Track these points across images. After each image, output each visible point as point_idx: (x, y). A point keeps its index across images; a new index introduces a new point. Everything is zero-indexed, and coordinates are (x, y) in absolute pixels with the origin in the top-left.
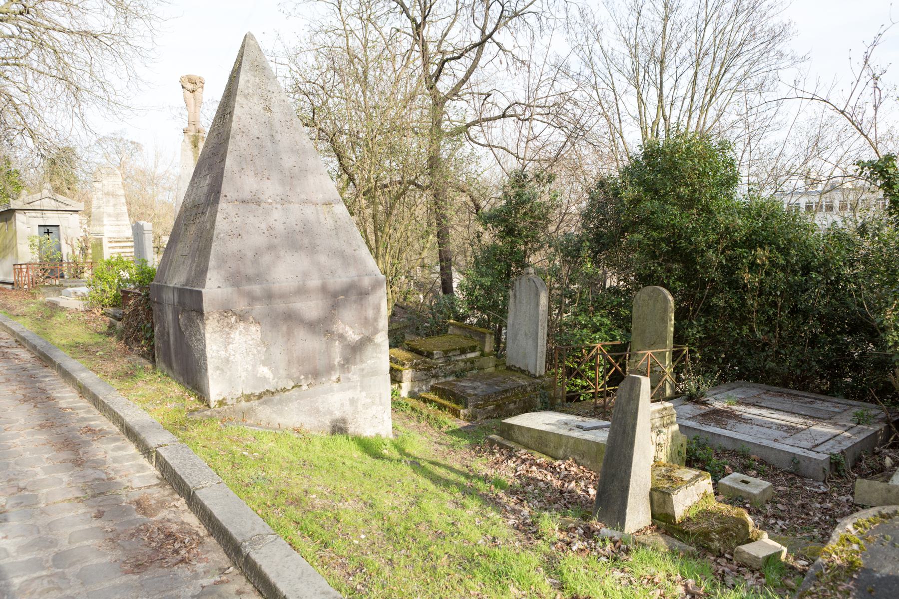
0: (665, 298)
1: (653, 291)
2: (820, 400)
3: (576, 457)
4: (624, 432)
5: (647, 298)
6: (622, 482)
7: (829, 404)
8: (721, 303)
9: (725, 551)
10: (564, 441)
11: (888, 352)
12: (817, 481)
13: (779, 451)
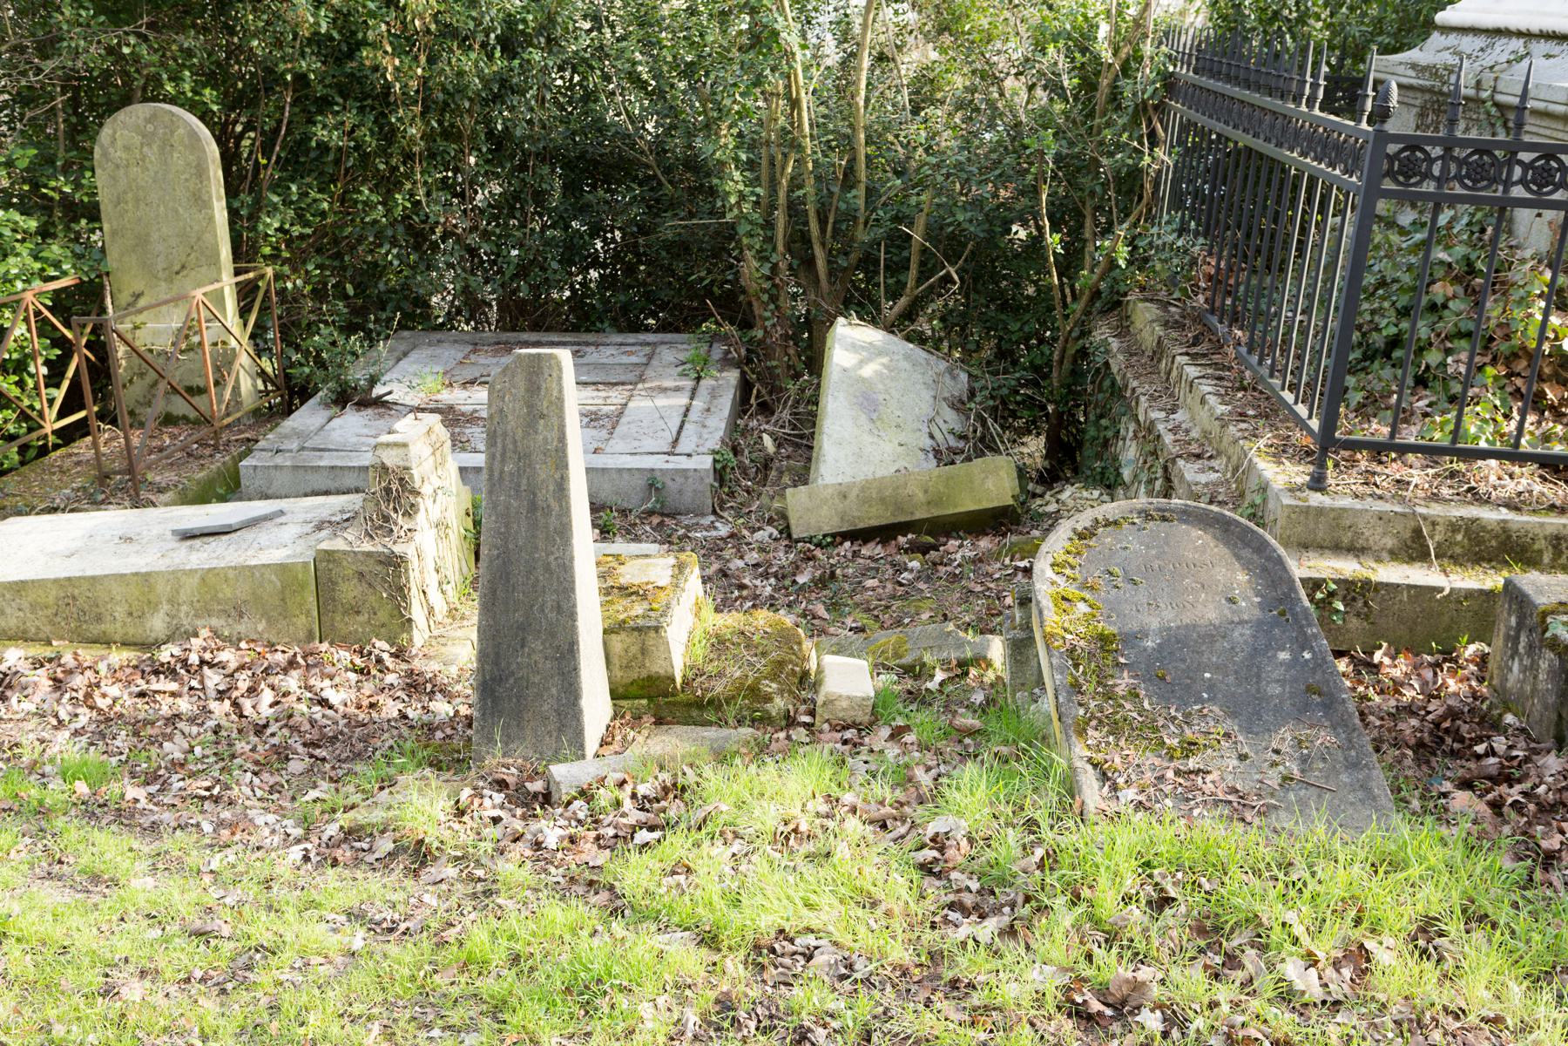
0: (193, 135)
1: (151, 119)
2: (587, 344)
3: (215, 622)
4: (533, 507)
5: (137, 140)
6: (553, 635)
7: (610, 351)
8: (336, 139)
9: (796, 712)
10: (163, 589)
11: (729, 218)
12: (703, 515)
13: (620, 471)
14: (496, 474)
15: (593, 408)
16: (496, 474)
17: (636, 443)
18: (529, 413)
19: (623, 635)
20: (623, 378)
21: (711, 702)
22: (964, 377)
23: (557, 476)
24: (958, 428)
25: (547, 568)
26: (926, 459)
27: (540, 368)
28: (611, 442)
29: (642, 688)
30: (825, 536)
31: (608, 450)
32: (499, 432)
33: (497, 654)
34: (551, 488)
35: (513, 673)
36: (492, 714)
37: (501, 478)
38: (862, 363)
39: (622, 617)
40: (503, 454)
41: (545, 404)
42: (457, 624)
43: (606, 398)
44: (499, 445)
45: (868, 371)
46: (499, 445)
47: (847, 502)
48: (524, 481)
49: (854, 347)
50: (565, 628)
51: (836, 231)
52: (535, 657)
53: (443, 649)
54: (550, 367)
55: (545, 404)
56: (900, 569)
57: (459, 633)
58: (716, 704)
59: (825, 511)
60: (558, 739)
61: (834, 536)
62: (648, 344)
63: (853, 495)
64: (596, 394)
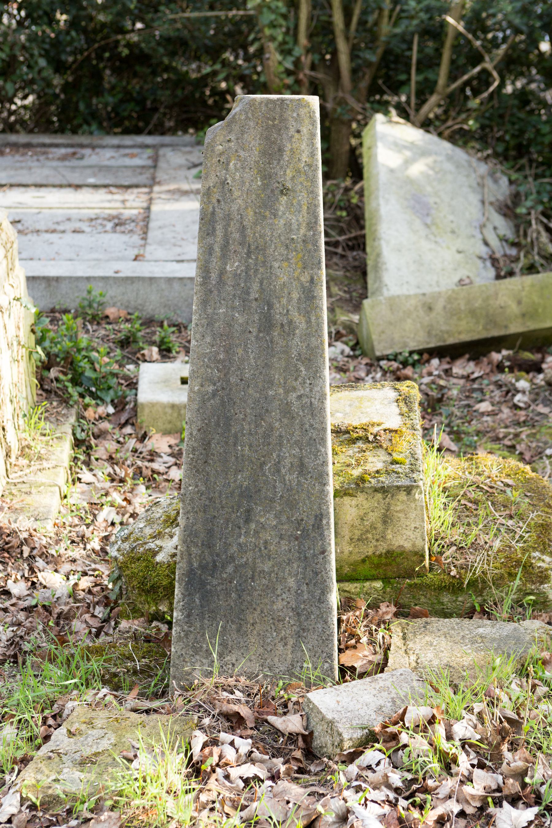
2: (82, 146)
4: (267, 323)
6: (292, 505)
7: (109, 153)
13: (170, 280)
14: (214, 276)
15: (114, 212)
16: (214, 276)
17: (178, 250)
18: (265, 187)
19: (361, 498)
20: (134, 181)
21: (472, 584)
22: (504, 181)
23: (305, 278)
24: (510, 235)
25: (286, 411)
26: (485, 267)
27: (283, 120)
28: (149, 248)
29: (377, 566)
30: (411, 353)
31: (148, 256)
32: (220, 214)
33: (210, 533)
34: (295, 295)
35: (232, 558)
36: (202, 616)
37: (221, 281)
38: (407, 163)
39: (356, 472)
40: (225, 247)
41: (289, 173)
42: (36, 465)
43: (124, 202)
44: (219, 233)
45: (418, 169)
46: (219, 233)
47: (433, 315)
48: (255, 286)
49: (398, 146)
50: (309, 495)
51: (362, 23)
52: (266, 536)
53: (28, 499)
54: (298, 119)
55: (289, 173)
56: (510, 391)
57: (41, 478)
58: (478, 585)
59: (409, 325)
60: (296, 647)
61: (420, 353)
62: (147, 146)
63: (439, 306)
64: (109, 197)
